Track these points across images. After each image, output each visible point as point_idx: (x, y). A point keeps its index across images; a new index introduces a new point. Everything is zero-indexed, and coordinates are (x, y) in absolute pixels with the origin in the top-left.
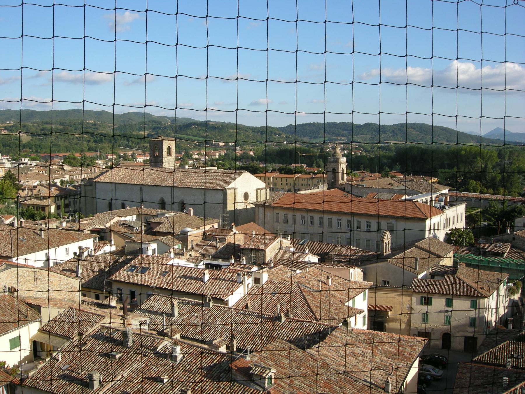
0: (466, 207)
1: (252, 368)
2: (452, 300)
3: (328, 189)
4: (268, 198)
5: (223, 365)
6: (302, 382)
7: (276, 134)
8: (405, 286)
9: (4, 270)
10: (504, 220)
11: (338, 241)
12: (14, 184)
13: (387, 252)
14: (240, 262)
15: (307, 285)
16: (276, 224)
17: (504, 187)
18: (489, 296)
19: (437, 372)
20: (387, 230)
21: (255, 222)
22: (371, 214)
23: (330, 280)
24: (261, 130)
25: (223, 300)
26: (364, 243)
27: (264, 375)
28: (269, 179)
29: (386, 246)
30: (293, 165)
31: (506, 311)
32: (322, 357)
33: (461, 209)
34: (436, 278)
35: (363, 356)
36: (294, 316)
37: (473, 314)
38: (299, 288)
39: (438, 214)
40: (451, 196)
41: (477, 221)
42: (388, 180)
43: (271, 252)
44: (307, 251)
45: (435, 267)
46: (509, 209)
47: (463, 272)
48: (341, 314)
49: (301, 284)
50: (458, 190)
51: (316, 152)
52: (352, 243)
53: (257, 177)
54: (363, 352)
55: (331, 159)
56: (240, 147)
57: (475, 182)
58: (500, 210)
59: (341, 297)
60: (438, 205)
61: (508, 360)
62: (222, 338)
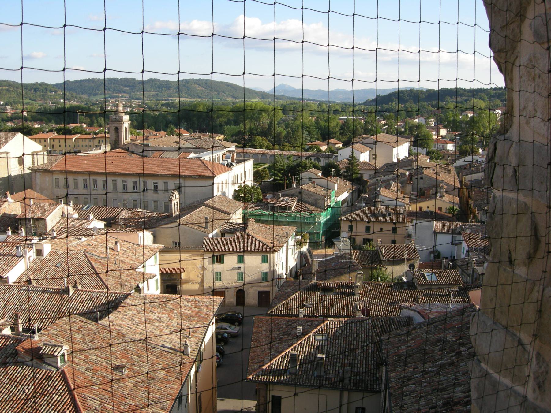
0: (253, 164)
1: (41, 348)
2: (243, 256)
3: (111, 149)
4: (46, 162)
5: (9, 349)
6: (98, 356)
7: (51, 92)
8: (198, 246)
10: (290, 175)
11: (124, 204)
13: (175, 213)
14: (19, 234)
15: (94, 253)
16: (56, 189)
17: (288, 142)
18: (279, 250)
19: (234, 329)
20: (175, 189)
21: (32, 189)
22: (191, 176)
23: (119, 245)
24: (35, 87)
25: (2, 277)
26: (151, 205)
27: (56, 354)
28: (45, 141)
29: (175, 206)
30: (71, 125)
31: (295, 263)
32: (117, 328)
33: (249, 165)
34: (227, 236)
35: (159, 321)
36: (83, 287)
37: (265, 268)
38: (86, 257)
39: (226, 171)
40: (238, 153)
41: (264, 177)
42: (175, 138)
43: (52, 220)
44: (92, 217)
45: (225, 225)
46: (295, 163)
47: (253, 228)
48: (132, 281)
49: (87, 252)
50: (244, 146)
51: (97, 111)
52: (139, 205)
53: (31, 139)
54: (158, 317)
55: (113, 117)
56: (11, 106)
57: (261, 138)
58: (285, 166)
59: (131, 262)
60: (226, 163)
61: (300, 310)
62: (5, 319)
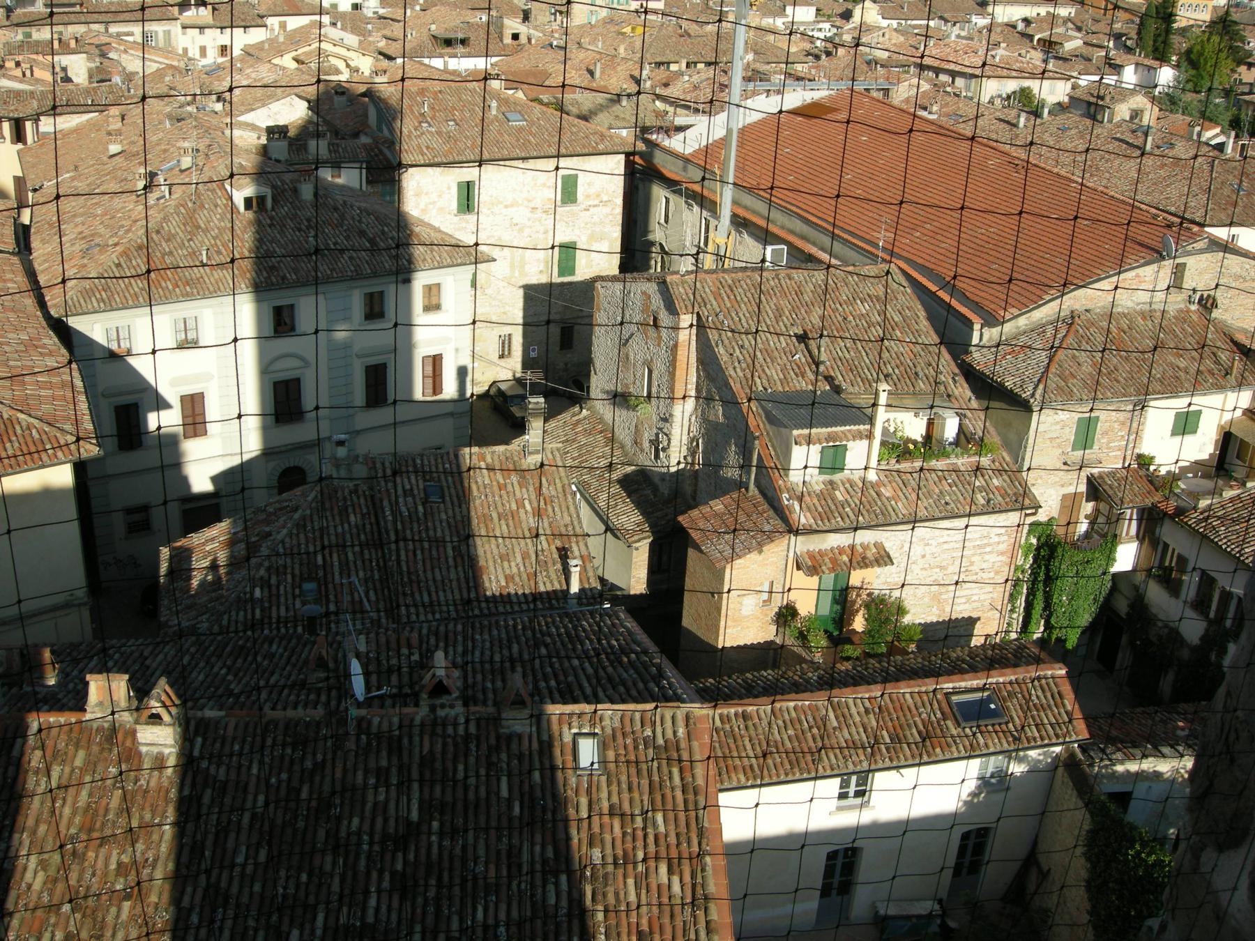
9: (1202, 251)
12: (1231, 48)
